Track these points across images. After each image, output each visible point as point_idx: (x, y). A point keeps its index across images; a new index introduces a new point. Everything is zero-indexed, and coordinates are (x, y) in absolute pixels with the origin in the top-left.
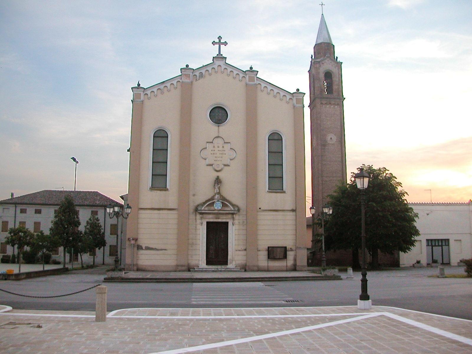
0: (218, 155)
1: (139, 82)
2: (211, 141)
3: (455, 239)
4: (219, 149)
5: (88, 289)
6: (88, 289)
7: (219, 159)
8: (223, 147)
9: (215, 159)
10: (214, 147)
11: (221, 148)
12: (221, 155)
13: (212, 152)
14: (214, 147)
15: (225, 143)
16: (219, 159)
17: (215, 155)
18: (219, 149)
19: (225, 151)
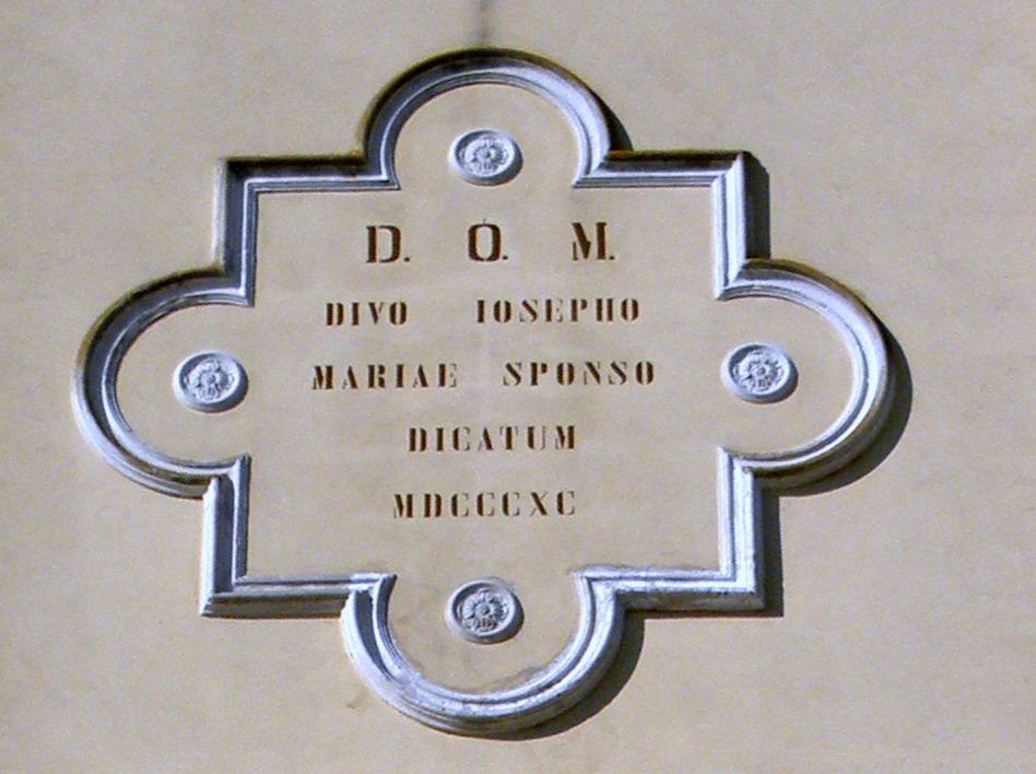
0: (483, 395)
1: (387, 261)
2: (347, 143)
3: (575, 430)
4: (494, 282)
5: (544, 439)
6: (544, 439)
7: (487, 472)
8: (590, 243)
9: (425, 474)
10: (384, 244)
11: (538, 268)
12: (548, 401)
13: (344, 347)
14: (384, 244)
15: (621, 151)
16: (487, 472)
17: (413, 405)
18: (494, 282)
19: (632, 309)
